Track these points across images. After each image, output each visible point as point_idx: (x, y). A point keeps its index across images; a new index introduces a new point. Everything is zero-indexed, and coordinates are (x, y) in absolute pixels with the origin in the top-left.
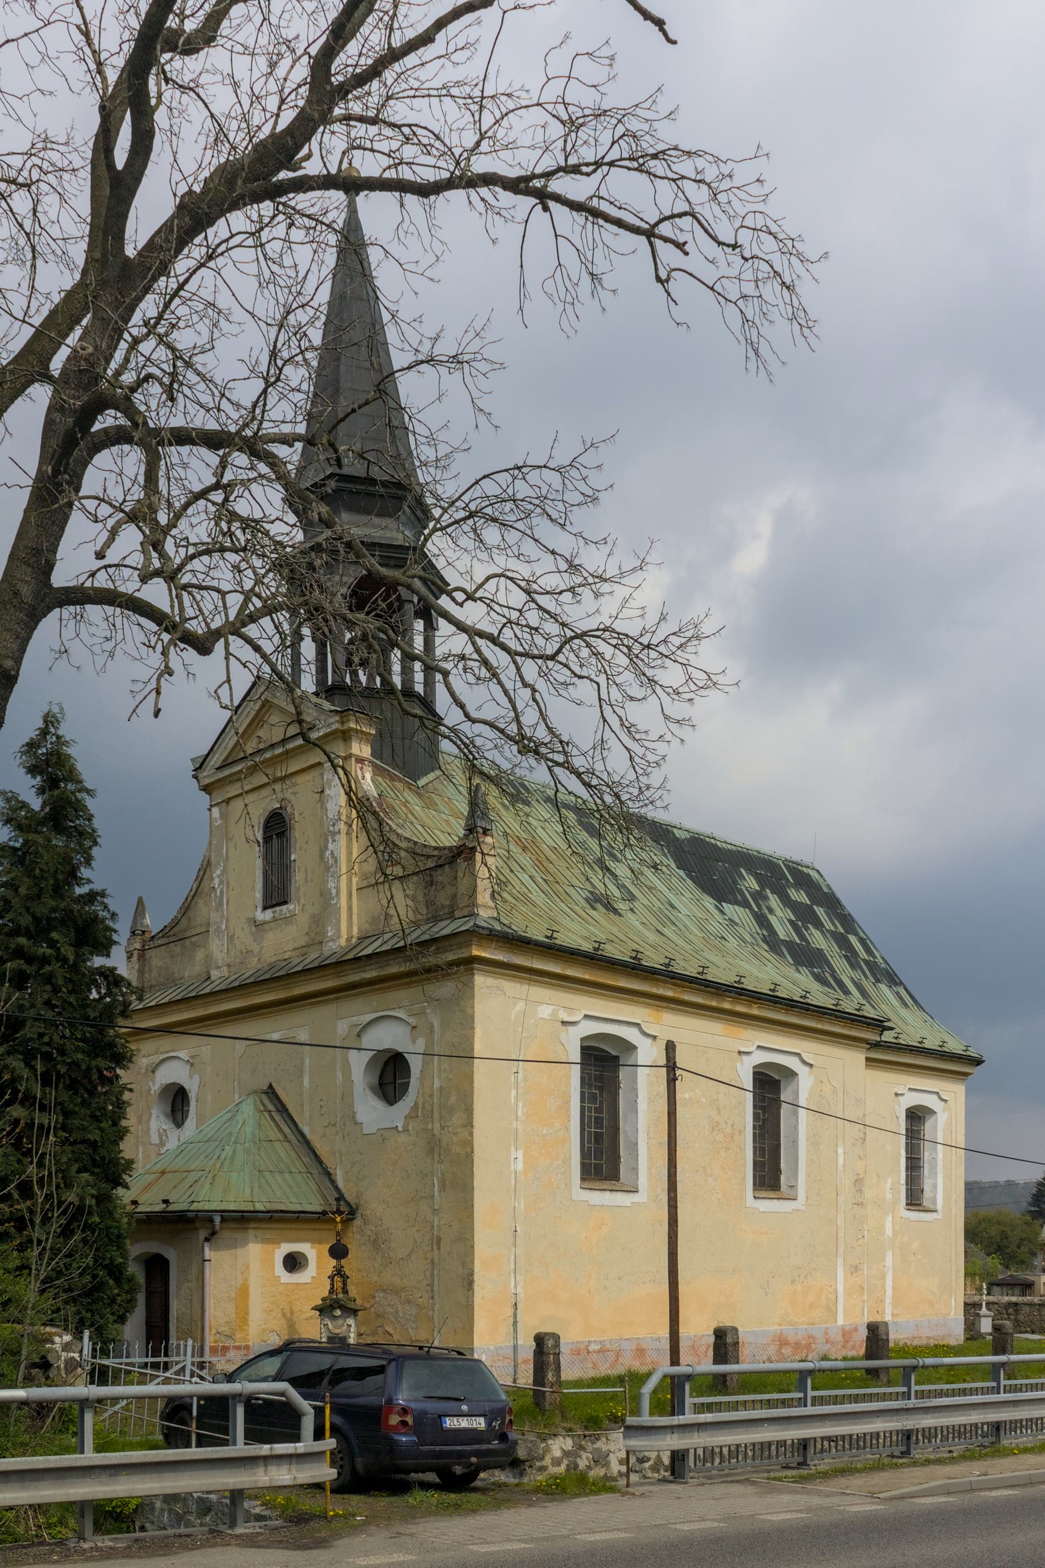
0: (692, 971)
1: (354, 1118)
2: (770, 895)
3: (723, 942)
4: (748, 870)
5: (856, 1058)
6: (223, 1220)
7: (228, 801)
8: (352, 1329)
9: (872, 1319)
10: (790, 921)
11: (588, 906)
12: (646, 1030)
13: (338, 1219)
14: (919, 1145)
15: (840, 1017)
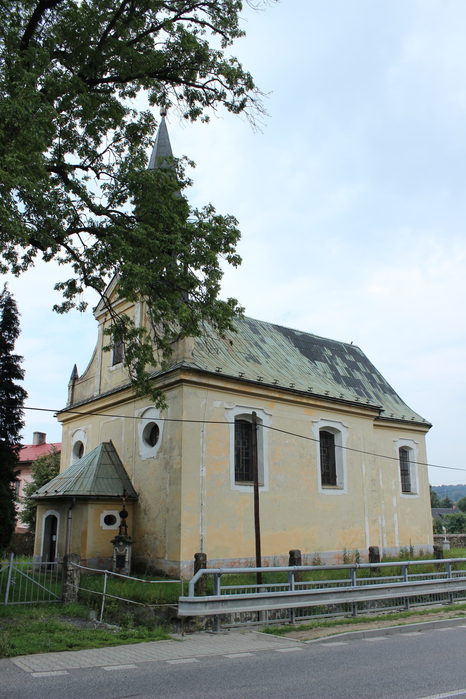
0: (288, 386)
1: (139, 453)
2: (337, 358)
3: (309, 375)
4: (327, 348)
5: (371, 422)
6: (77, 499)
8: (128, 552)
9: (372, 545)
10: (346, 368)
11: (246, 360)
13: (124, 499)
14: (407, 464)
15: (359, 406)
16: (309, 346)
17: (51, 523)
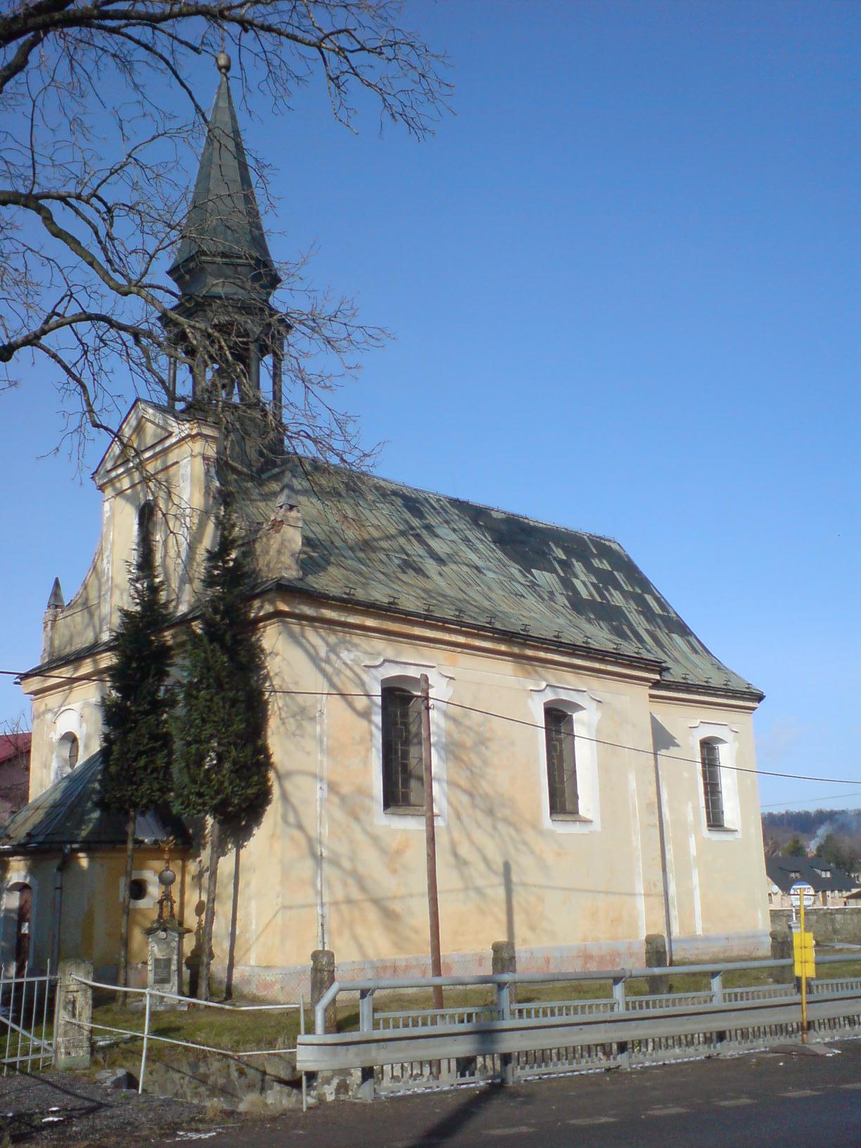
16: (521, 541)
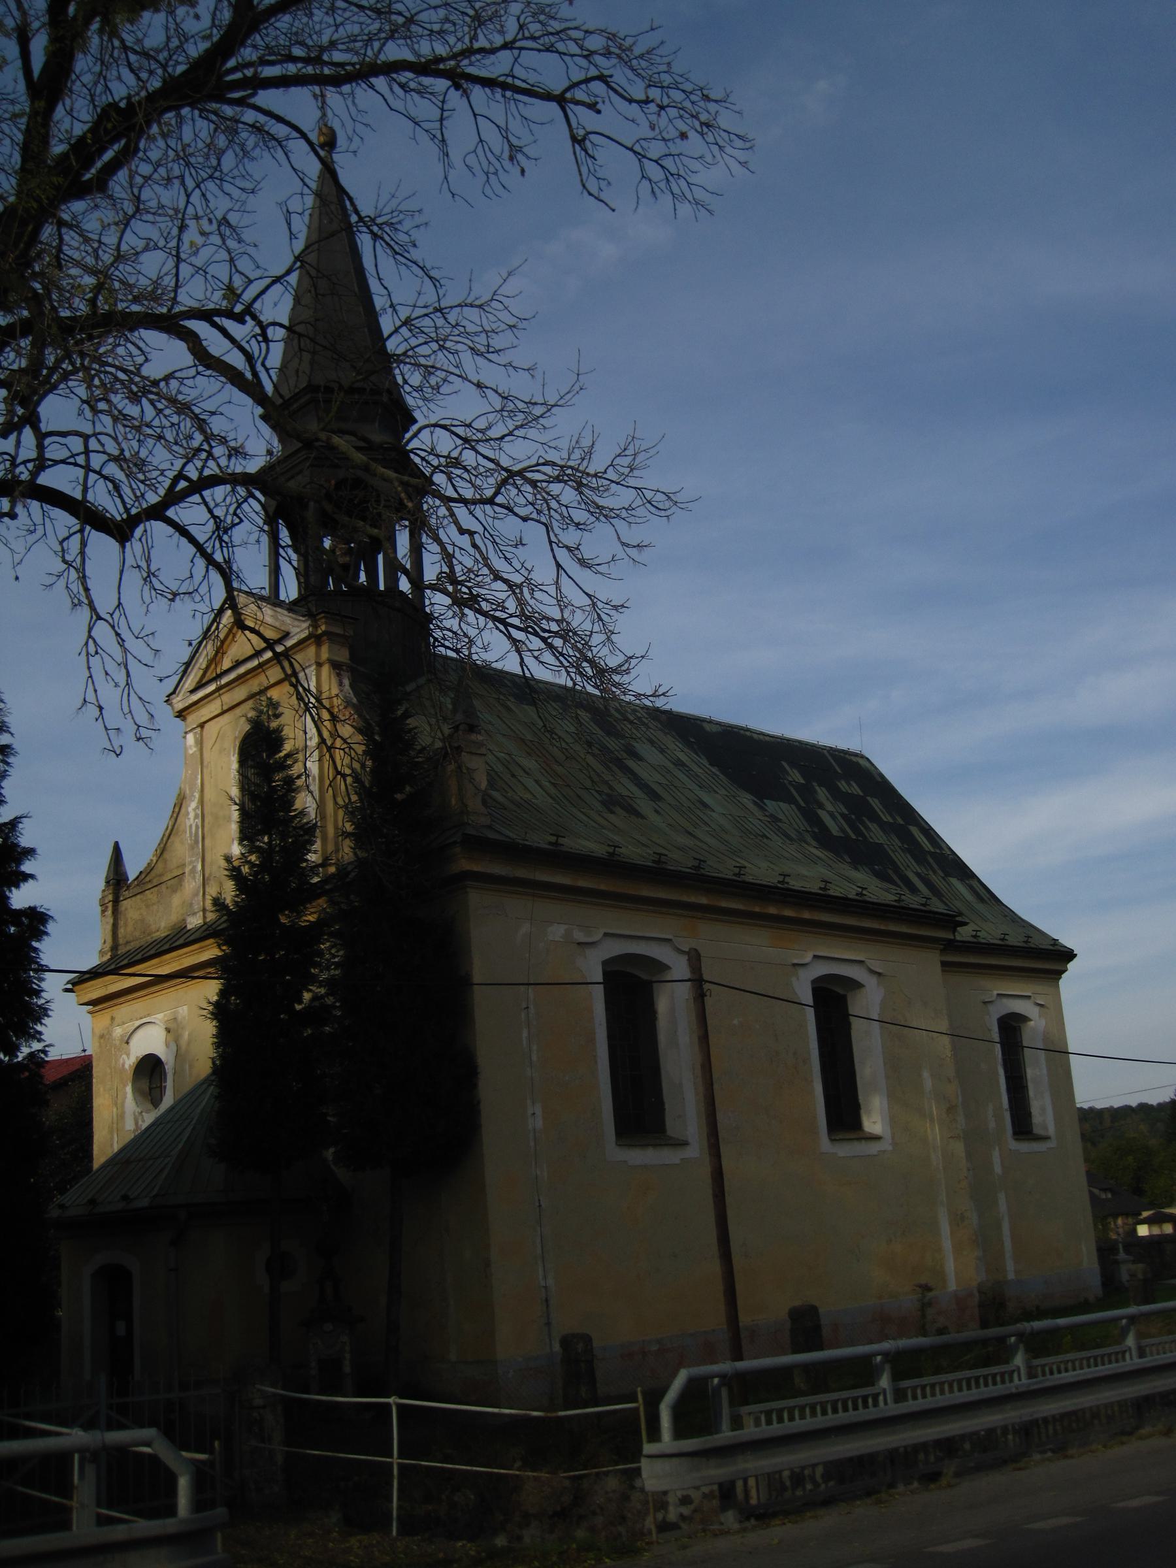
5: (931, 960)
7: (202, 726)
10: (842, 815)
12: (664, 942)
17: (114, 1285)
